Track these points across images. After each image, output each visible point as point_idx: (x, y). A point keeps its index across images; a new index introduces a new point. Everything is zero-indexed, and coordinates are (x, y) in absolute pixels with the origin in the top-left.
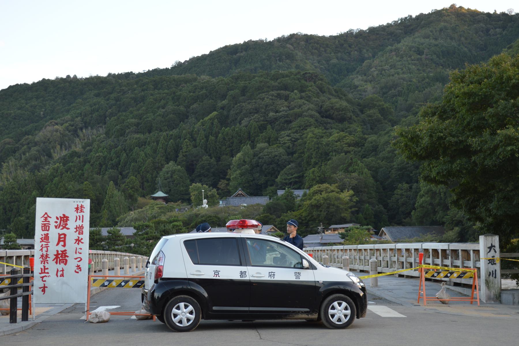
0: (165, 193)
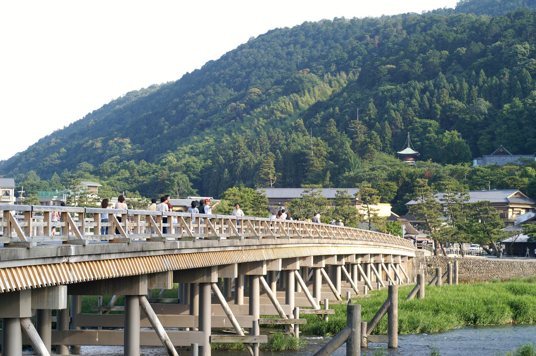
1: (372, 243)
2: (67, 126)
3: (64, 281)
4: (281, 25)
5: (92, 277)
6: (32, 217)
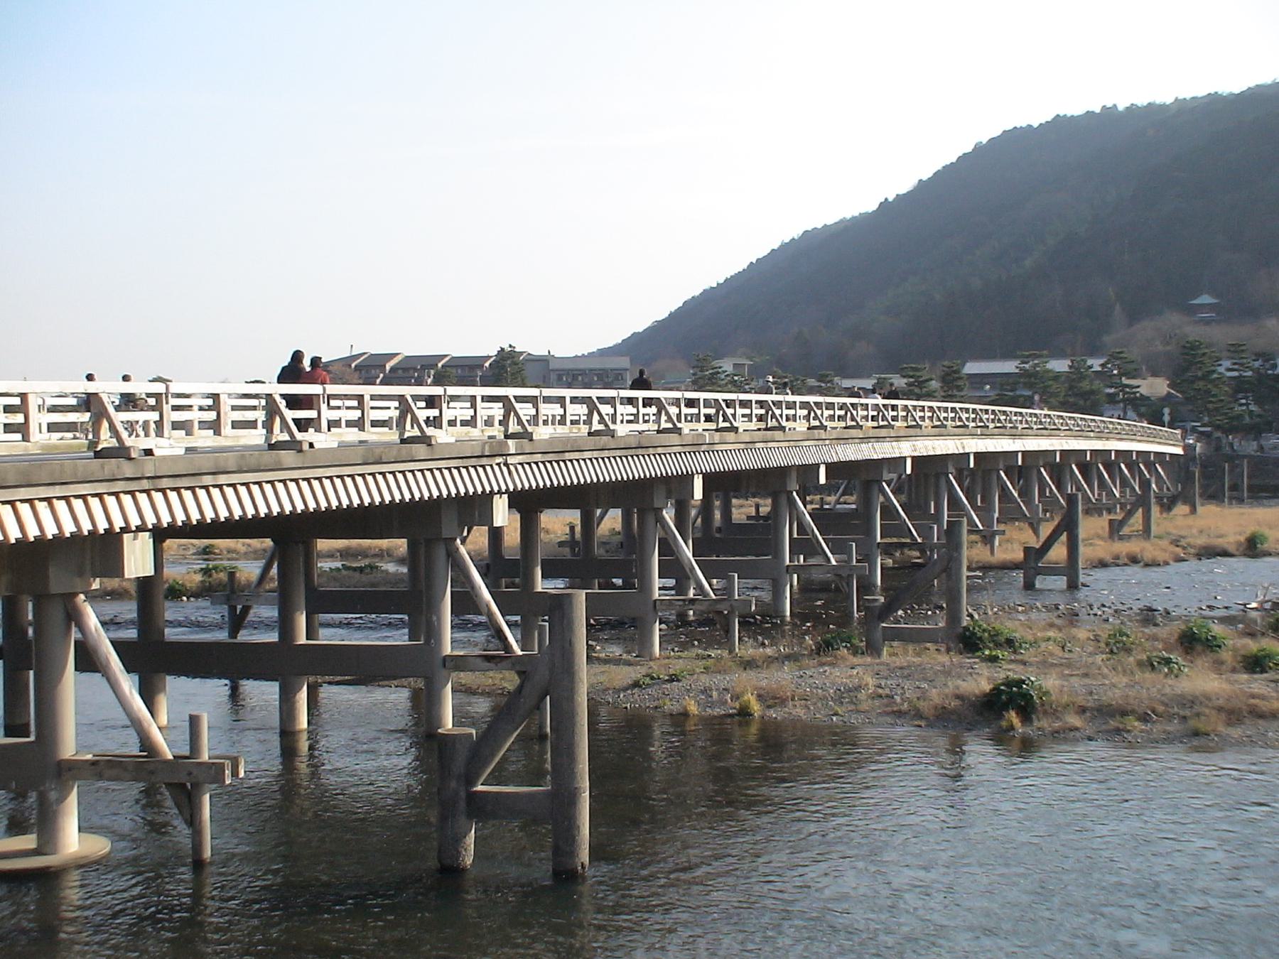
0: (1217, 297)
1: (1092, 434)
2: (721, 281)
3: (504, 488)
4: (1022, 123)
5: (548, 484)
6: (167, 403)
